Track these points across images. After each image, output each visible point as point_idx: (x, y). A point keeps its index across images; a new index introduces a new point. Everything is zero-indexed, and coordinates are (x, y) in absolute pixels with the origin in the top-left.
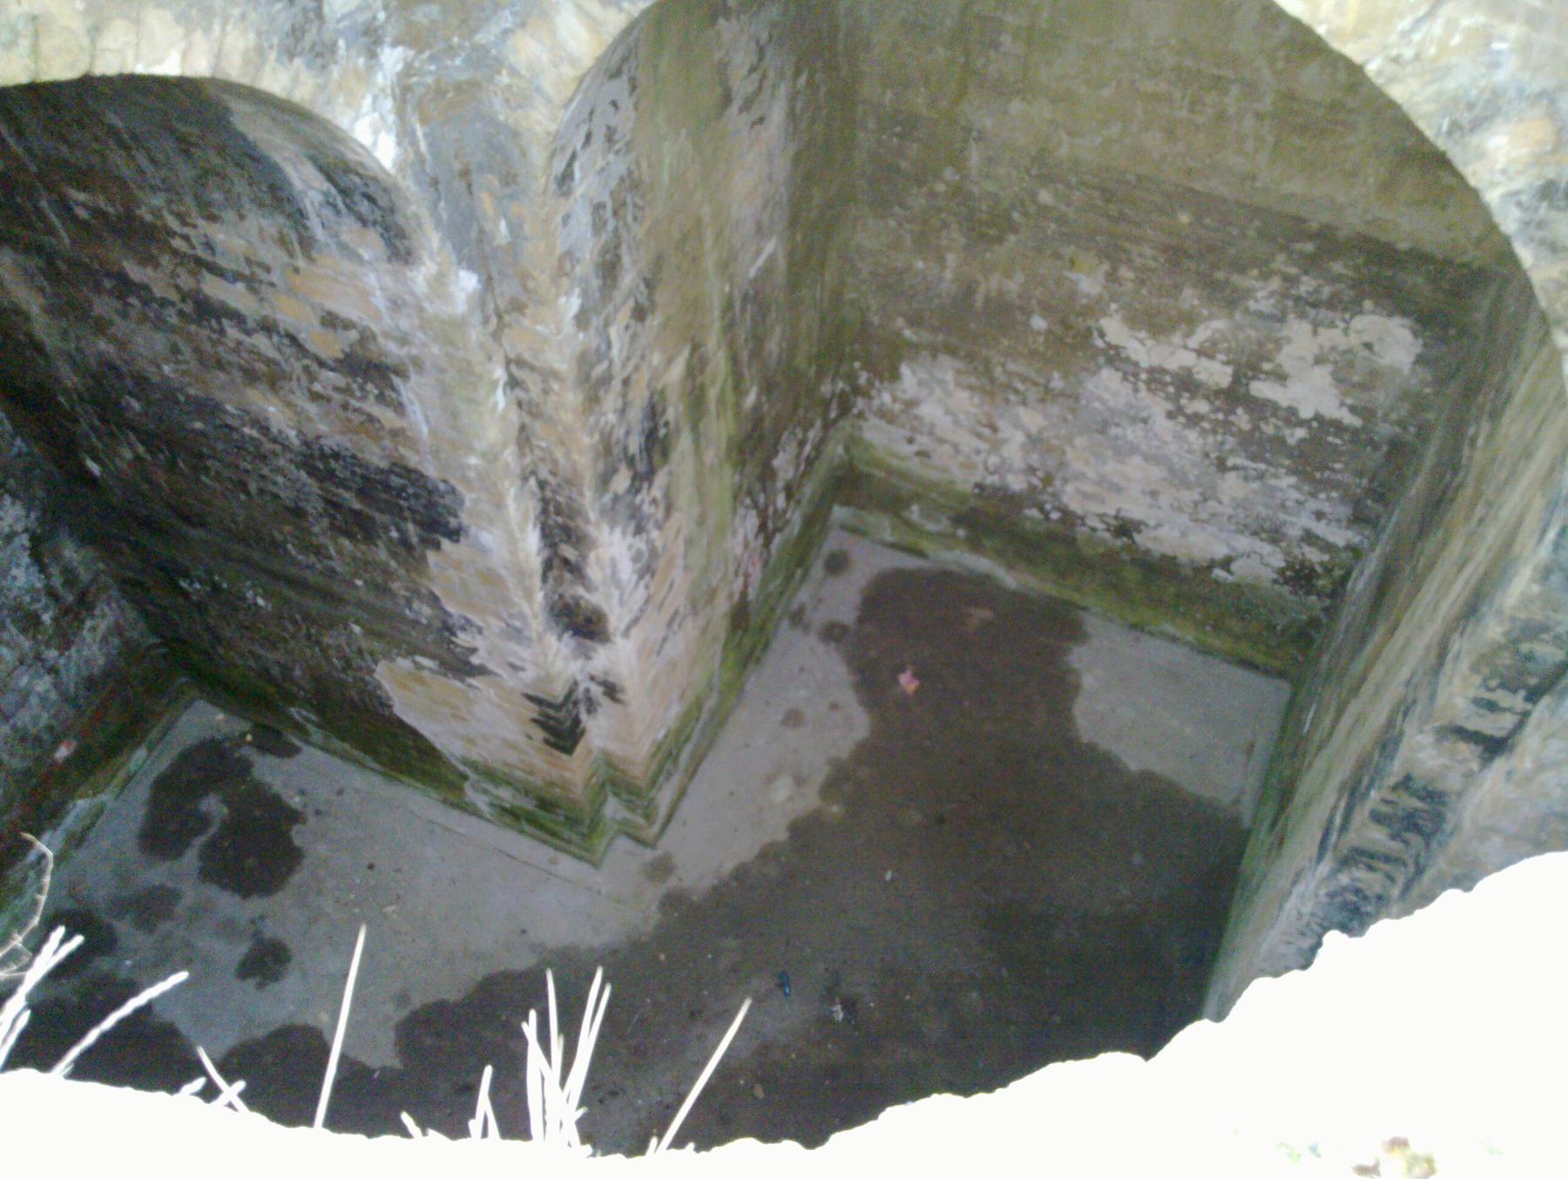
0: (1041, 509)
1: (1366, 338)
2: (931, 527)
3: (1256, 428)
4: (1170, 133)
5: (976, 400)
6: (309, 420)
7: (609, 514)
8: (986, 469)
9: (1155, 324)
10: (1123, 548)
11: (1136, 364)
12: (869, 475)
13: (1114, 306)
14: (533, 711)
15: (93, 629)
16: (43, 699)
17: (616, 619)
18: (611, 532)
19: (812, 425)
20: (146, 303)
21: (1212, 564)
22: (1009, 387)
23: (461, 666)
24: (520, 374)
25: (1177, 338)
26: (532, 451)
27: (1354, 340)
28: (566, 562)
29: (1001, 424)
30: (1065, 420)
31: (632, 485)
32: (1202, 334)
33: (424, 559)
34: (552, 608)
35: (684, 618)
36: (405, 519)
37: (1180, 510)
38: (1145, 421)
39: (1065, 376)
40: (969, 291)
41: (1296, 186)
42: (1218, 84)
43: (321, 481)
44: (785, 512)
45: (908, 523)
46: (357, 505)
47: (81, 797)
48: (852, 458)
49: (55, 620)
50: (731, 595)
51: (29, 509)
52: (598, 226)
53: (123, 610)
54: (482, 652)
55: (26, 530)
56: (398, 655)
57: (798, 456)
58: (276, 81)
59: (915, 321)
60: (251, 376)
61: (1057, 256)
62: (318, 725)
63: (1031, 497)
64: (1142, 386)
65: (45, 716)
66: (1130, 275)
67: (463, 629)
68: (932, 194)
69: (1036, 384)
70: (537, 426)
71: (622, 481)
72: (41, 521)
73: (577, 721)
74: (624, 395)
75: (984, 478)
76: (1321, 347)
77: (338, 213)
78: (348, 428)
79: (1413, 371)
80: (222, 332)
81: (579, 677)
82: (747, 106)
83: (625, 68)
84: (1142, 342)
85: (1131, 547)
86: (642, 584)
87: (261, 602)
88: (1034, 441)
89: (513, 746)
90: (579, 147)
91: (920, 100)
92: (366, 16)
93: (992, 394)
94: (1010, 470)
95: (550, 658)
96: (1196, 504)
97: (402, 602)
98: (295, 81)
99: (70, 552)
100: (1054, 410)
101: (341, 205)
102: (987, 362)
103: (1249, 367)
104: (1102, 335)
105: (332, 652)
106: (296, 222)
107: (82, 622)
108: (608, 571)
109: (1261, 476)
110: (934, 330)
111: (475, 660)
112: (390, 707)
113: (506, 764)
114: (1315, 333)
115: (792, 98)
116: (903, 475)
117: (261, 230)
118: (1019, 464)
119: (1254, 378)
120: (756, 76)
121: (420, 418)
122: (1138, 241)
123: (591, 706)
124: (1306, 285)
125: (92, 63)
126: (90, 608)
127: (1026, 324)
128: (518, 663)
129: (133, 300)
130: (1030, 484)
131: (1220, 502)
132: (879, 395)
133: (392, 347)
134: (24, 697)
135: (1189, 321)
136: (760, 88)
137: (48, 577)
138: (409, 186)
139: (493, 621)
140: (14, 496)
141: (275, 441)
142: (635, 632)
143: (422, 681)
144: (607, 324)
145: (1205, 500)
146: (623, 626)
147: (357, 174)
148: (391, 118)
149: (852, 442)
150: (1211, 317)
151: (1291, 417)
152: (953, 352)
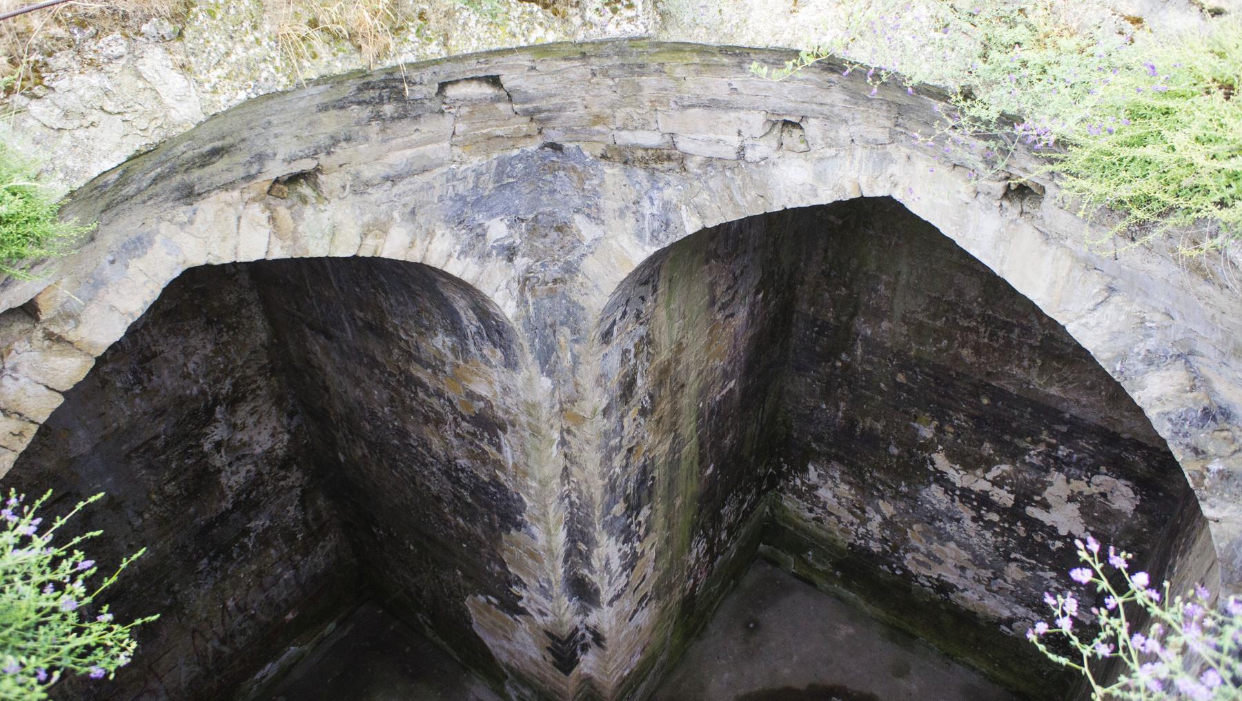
0: (890, 567)
1: (1102, 489)
2: (819, 567)
3: (1029, 536)
4: (977, 350)
5: (853, 492)
6: (452, 447)
7: (609, 527)
8: (857, 535)
9: (969, 463)
10: (941, 601)
11: (954, 484)
12: (784, 528)
13: (940, 447)
14: (548, 642)
17: (606, 594)
18: (609, 538)
19: (750, 492)
20: (382, 373)
21: (1000, 621)
22: (874, 486)
23: (512, 606)
24: (567, 438)
25: (979, 472)
26: (569, 483)
27: (1094, 490)
28: (580, 552)
29: (868, 508)
30: (908, 513)
31: (626, 512)
32: (995, 472)
33: (500, 537)
34: (568, 580)
35: (650, 600)
36: (493, 513)
37: (979, 581)
38: (958, 520)
39: (908, 485)
40: (852, 423)
41: (1054, 390)
42: (1008, 327)
43: (453, 483)
44: (726, 542)
45: (805, 561)
46: (469, 500)
47: (293, 645)
48: (774, 515)
50: (684, 590)
52: (624, 361)
54: (525, 600)
55: (300, 486)
56: (479, 592)
57: (738, 509)
58: (455, 268)
59: (819, 439)
61: (907, 413)
62: (431, 627)
63: (883, 557)
64: (957, 498)
65: (285, 593)
66: (951, 430)
67: (516, 584)
68: (834, 366)
69: (891, 487)
70: (574, 469)
71: (619, 509)
73: (574, 654)
74: (627, 458)
75: (855, 541)
76: (1072, 491)
77: (483, 338)
78: (472, 456)
79: (1134, 515)
80: (416, 393)
81: (580, 627)
82: (723, 308)
83: (651, 280)
84: (957, 471)
85: (947, 601)
86: (625, 574)
87: (412, 547)
88: (887, 523)
89: (535, 663)
90: (618, 318)
91: (830, 315)
92: (511, 240)
93: (863, 489)
94: (872, 538)
95: (562, 611)
96: (989, 579)
97: (485, 560)
98: (465, 269)
99: (320, 502)
100: (902, 505)
101: (485, 335)
102: (861, 468)
103: (1027, 494)
104: (933, 463)
105: (444, 584)
106: (461, 340)
108: (604, 563)
109: (1033, 568)
110: (830, 445)
111: (520, 604)
112: (471, 624)
113: (530, 673)
114: (1068, 482)
115: (753, 305)
116: (804, 531)
117: (444, 342)
118: (878, 536)
119: (1028, 504)
120: (731, 292)
121: (509, 455)
122: (957, 410)
123: (585, 648)
124: (1062, 451)
125: (376, 251)
127: (886, 449)
128: (544, 610)
129: (377, 371)
130: (884, 549)
131: (1005, 581)
132: (794, 479)
133: (500, 414)
135: (988, 464)
136: (733, 298)
138: (518, 327)
139: (533, 581)
141: (433, 457)
142: (616, 603)
143: (489, 611)
144: (622, 417)
145: (996, 578)
146: (609, 597)
147: (494, 320)
148: (516, 293)
149: (776, 505)
150: (1001, 462)
151: (1052, 532)
152: (840, 460)
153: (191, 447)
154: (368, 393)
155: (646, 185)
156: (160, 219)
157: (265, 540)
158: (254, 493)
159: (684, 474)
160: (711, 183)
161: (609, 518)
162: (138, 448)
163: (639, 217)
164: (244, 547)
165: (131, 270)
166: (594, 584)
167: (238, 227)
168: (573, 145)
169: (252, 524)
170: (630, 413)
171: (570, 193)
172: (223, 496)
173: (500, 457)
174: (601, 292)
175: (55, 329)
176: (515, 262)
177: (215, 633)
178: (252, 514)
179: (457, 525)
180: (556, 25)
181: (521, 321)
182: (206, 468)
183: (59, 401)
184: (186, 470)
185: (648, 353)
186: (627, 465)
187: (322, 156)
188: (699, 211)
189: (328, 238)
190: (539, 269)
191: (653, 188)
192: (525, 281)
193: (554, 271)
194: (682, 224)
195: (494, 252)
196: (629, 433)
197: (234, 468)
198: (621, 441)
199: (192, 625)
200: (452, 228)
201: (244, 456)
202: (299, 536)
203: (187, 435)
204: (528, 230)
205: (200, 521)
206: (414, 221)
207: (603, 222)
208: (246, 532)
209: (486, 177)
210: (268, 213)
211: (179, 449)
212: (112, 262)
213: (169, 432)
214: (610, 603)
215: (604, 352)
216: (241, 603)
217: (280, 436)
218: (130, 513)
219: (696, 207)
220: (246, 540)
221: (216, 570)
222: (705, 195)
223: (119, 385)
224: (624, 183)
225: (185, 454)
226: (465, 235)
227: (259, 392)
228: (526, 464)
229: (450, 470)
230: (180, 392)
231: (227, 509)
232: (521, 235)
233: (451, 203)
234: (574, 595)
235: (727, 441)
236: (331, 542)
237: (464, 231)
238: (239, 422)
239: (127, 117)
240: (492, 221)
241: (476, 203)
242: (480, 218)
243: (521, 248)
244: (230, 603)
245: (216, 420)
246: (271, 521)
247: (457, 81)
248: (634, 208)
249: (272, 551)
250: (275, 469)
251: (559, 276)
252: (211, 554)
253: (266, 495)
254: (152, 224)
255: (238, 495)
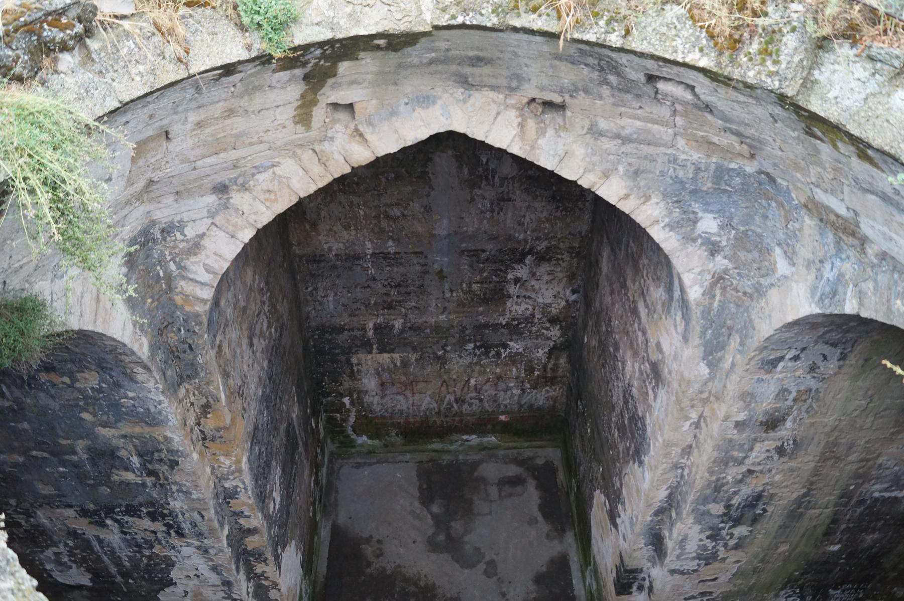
7: (700, 516)
14: (618, 562)
15: (548, 391)
16: (512, 395)
24: (703, 424)
31: (722, 516)
34: (651, 529)
46: (626, 422)
49: (538, 376)
51: (562, 336)
53: (562, 395)
58: (657, 234)
60: (631, 347)
70: (695, 451)
71: (717, 509)
72: (562, 344)
78: (640, 389)
92: (718, 239)
99: (562, 361)
107: (546, 385)
126: (552, 384)
134: (508, 389)
137: (549, 362)
140: (561, 328)
142: (677, 576)
144: (755, 440)
153: (501, 270)
154: (613, 304)
155: (833, 251)
156: (445, 91)
157: (514, 359)
158: (523, 325)
159: (802, 530)
160: (879, 277)
161: (702, 508)
162: (471, 251)
163: (819, 277)
164: (498, 355)
165: (416, 114)
166: (666, 547)
167: (495, 118)
168: (785, 183)
169: (511, 344)
170: (766, 443)
171: (778, 225)
172: (503, 314)
173: (653, 405)
174: (770, 323)
175: (361, 128)
176: (717, 259)
177: (455, 391)
178: (514, 337)
179: (613, 435)
180: (713, 54)
181: (701, 308)
182: (502, 290)
183: (348, 170)
184: (490, 282)
185: (811, 406)
186: (741, 481)
187: (567, 97)
188: (861, 296)
189: (557, 158)
190: (735, 275)
191: (836, 255)
192: (719, 279)
193: (747, 285)
194: (844, 300)
195: (699, 241)
196: (757, 457)
197: (519, 301)
198: (745, 458)
199: (445, 377)
200: (668, 203)
201: (529, 297)
202: (536, 373)
203: (502, 261)
204: (736, 238)
205: (482, 320)
206: (635, 180)
207: (794, 265)
208: (505, 346)
209: (705, 174)
210: (520, 120)
211: (493, 267)
212: (407, 104)
213: (493, 252)
214: (673, 572)
215: (761, 376)
216: (479, 386)
217: (560, 300)
218: (447, 286)
219: (860, 292)
220: (502, 351)
221: (475, 355)
222: (871, 285)
223: (480, 206)
224: (817, 238)
225: (495, 272)
226: (677, 213)
227: (561, 262)
228: (663, 421)
229: (627, 394)
230: (512, 232)
231: (501, 324)
232: (728, 239)
233: (671, 182)
234: (651, 544)
235: (869, 538)
236: (555, 391)
237: (677, 210)
238: (538, 274)
239: (392, 8)
240: (706, 215)
241: (694, 192)
242: (696, 206)
243: (725, 249)
244: (473, 382)
245: (524, 263)
246: (524, 350)
247: (670, 80)
248: (818, 265)
249: (514, 369)
250: (545, 319)
251: (749, 291)
252: (478, 344)
253: (530, 332)
254: (439, 91)
255: (513, 320)
